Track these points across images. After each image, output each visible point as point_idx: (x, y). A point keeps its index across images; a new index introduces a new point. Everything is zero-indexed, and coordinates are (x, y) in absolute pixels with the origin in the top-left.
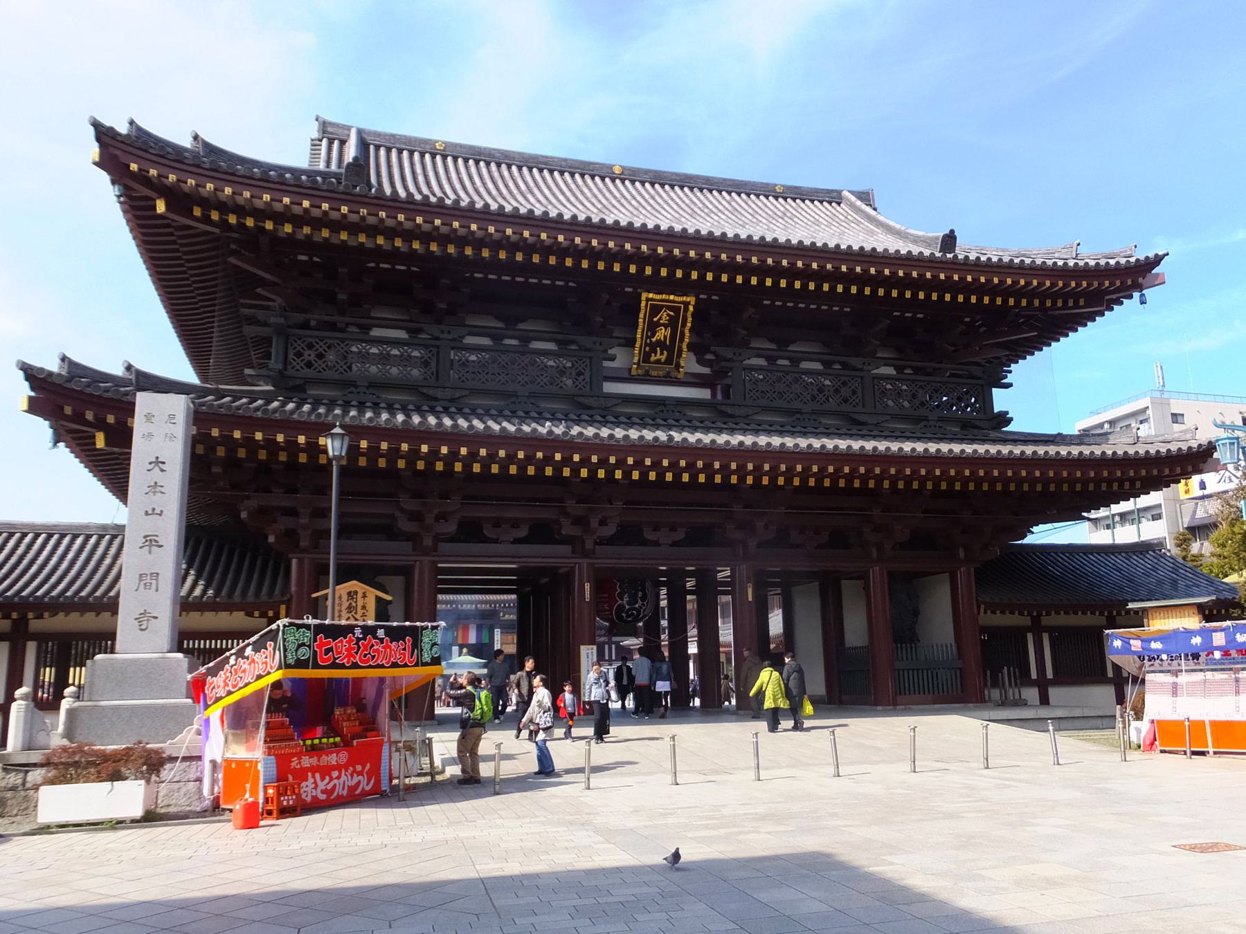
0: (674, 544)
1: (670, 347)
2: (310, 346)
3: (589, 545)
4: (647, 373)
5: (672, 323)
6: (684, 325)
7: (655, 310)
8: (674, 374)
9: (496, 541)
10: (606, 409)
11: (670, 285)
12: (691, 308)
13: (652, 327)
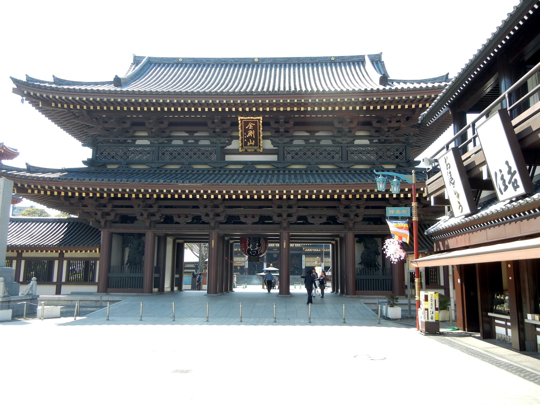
0: (254, 223)
1: (256, 139)
2: (191, 150)
5: (255, 128)
6: (259, 129)
8: (258, 150)
9: (313, 224)
10: (284, 168)
11: (251, 113)
12: (261, 122)
13: (246, 131)
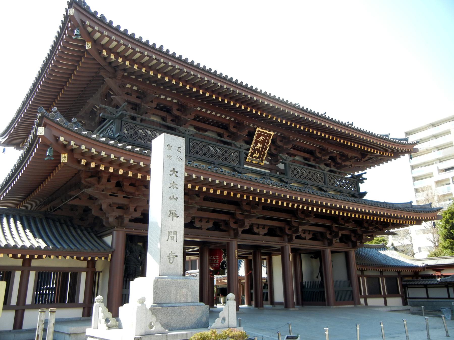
0: (208, 229)
3: (126, 221)
4: (251, 162)
5: (263, 142)
6: (268, 143)
7: (259, 135)
12: (272, 137)
